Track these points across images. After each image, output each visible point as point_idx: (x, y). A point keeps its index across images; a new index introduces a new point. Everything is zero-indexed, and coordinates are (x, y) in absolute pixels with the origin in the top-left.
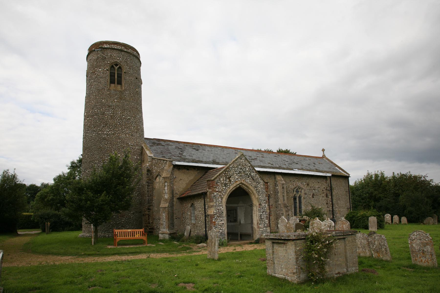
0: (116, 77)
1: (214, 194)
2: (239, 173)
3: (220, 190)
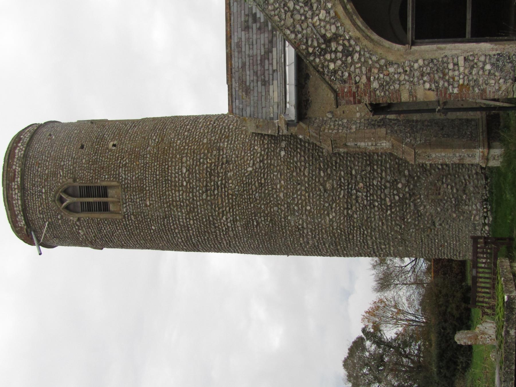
0: (91, 200)
1: (375, 90)
2: (311, 8)
3: (364, 69)
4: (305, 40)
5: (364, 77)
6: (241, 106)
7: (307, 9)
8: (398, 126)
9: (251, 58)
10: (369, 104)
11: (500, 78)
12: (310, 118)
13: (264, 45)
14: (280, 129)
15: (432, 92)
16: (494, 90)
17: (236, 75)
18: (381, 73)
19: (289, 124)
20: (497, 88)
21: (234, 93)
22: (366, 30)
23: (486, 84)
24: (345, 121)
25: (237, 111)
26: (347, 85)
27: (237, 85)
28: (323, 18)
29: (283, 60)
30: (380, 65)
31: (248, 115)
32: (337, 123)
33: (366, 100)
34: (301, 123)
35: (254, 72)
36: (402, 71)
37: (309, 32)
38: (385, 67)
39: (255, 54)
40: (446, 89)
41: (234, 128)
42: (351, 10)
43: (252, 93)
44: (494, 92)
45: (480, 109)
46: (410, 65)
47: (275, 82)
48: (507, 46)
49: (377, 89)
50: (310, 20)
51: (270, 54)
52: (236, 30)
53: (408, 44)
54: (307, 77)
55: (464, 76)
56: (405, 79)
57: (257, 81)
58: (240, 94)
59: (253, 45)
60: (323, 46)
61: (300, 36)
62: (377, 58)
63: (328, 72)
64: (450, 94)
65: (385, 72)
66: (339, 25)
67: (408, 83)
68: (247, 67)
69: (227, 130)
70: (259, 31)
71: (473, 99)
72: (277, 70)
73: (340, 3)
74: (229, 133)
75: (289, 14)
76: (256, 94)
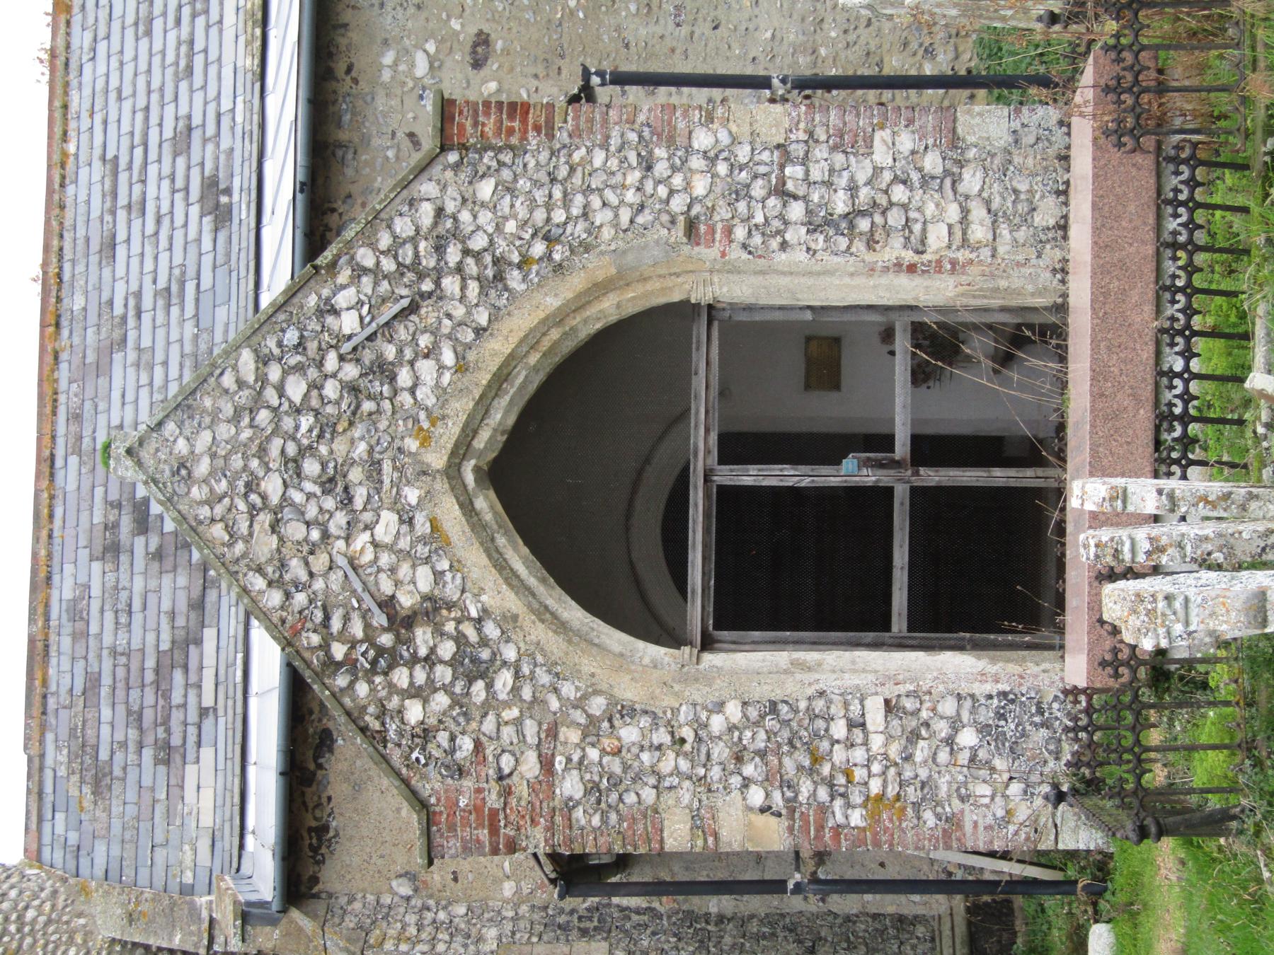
1: (569, 805)
3: (530, 728)
4: (319, 616)
5: (531, 759)
6: (73, 837)
7: (329, 503)
8: (654, 934)
9: (123, 660)
10: (548, 855)
11: (1011, 778)
12: (330, 896)
13: (172, 615)
14: (216, 932)
15: (773, 820)
16: (990, 820)
17: (62, 722)
18: (593, 745)
19: (248, 915)
20: (1000, 813)
21: (48, 788)
22: (541, 590)
23: (963, 799)
24: (461, 910)
25: (58, 855)
26: (468, 783)
27: (63, 758)
28: (388, 539)
29: (239, 673)
30: (588, 716)
31: (99, 872)
32: (429, 916)
33: (537, 839)
34: (295, 914)
35: (129, 712)
36: (667, 739)
37: (335, 587)
38: (606, 724)
39: (136, 645)
40: (823, 810)
41: (42, 919)
42: (488, 517)
43: (117, 787)
44: (988, 828)
45: (946, 885)
46: (697, 719)
47: (207, 753)
48: (1032, 669)
49: (578, 803)
50: (341, 544)
51: (193, 649)
52: (69, 555)
53: (691, 644)
54: (326, 741)
55: (887, 768)
56: (676, 771)
57: (140, 746)
58: (74, 792)
59: (130, 613)
60: (386, 640)
61: (300, 598)
62: (577, 689)
63: (400, 734)
64: (837, 829)
65: (607, 743)
66: (444, 565)
67: (687, 784)
68: (104, 691)
69: (13, 928)
70: (156, 565)
71: (917, 848)
72: (215, 710)
73: (453, 489)
74: (22, 939)
75: (265, 519)
76: (131, 795)
